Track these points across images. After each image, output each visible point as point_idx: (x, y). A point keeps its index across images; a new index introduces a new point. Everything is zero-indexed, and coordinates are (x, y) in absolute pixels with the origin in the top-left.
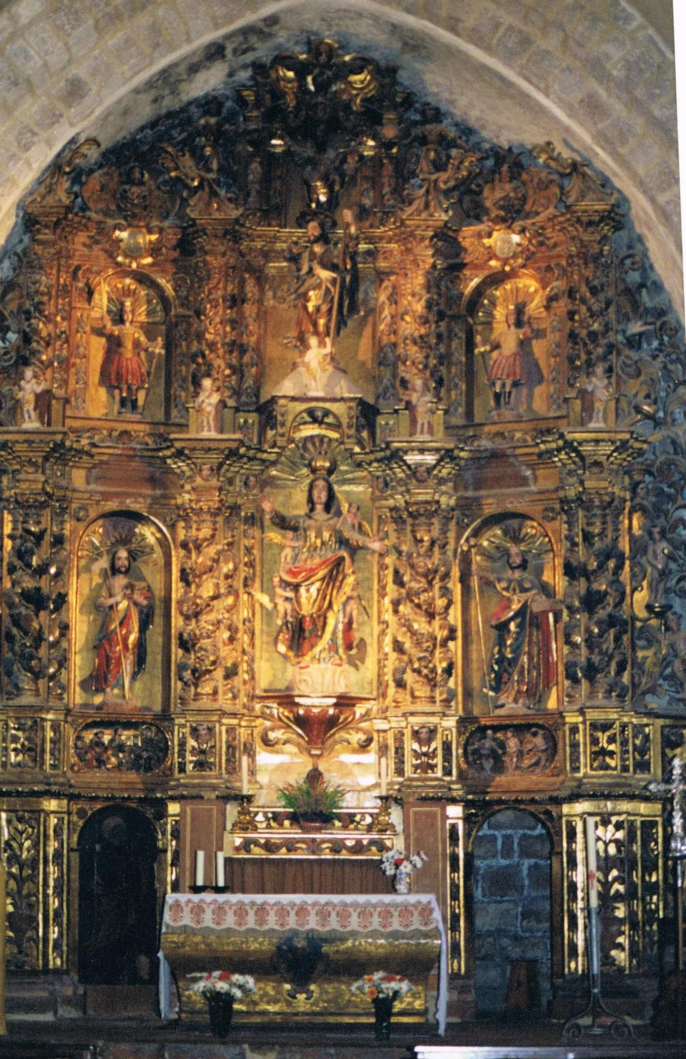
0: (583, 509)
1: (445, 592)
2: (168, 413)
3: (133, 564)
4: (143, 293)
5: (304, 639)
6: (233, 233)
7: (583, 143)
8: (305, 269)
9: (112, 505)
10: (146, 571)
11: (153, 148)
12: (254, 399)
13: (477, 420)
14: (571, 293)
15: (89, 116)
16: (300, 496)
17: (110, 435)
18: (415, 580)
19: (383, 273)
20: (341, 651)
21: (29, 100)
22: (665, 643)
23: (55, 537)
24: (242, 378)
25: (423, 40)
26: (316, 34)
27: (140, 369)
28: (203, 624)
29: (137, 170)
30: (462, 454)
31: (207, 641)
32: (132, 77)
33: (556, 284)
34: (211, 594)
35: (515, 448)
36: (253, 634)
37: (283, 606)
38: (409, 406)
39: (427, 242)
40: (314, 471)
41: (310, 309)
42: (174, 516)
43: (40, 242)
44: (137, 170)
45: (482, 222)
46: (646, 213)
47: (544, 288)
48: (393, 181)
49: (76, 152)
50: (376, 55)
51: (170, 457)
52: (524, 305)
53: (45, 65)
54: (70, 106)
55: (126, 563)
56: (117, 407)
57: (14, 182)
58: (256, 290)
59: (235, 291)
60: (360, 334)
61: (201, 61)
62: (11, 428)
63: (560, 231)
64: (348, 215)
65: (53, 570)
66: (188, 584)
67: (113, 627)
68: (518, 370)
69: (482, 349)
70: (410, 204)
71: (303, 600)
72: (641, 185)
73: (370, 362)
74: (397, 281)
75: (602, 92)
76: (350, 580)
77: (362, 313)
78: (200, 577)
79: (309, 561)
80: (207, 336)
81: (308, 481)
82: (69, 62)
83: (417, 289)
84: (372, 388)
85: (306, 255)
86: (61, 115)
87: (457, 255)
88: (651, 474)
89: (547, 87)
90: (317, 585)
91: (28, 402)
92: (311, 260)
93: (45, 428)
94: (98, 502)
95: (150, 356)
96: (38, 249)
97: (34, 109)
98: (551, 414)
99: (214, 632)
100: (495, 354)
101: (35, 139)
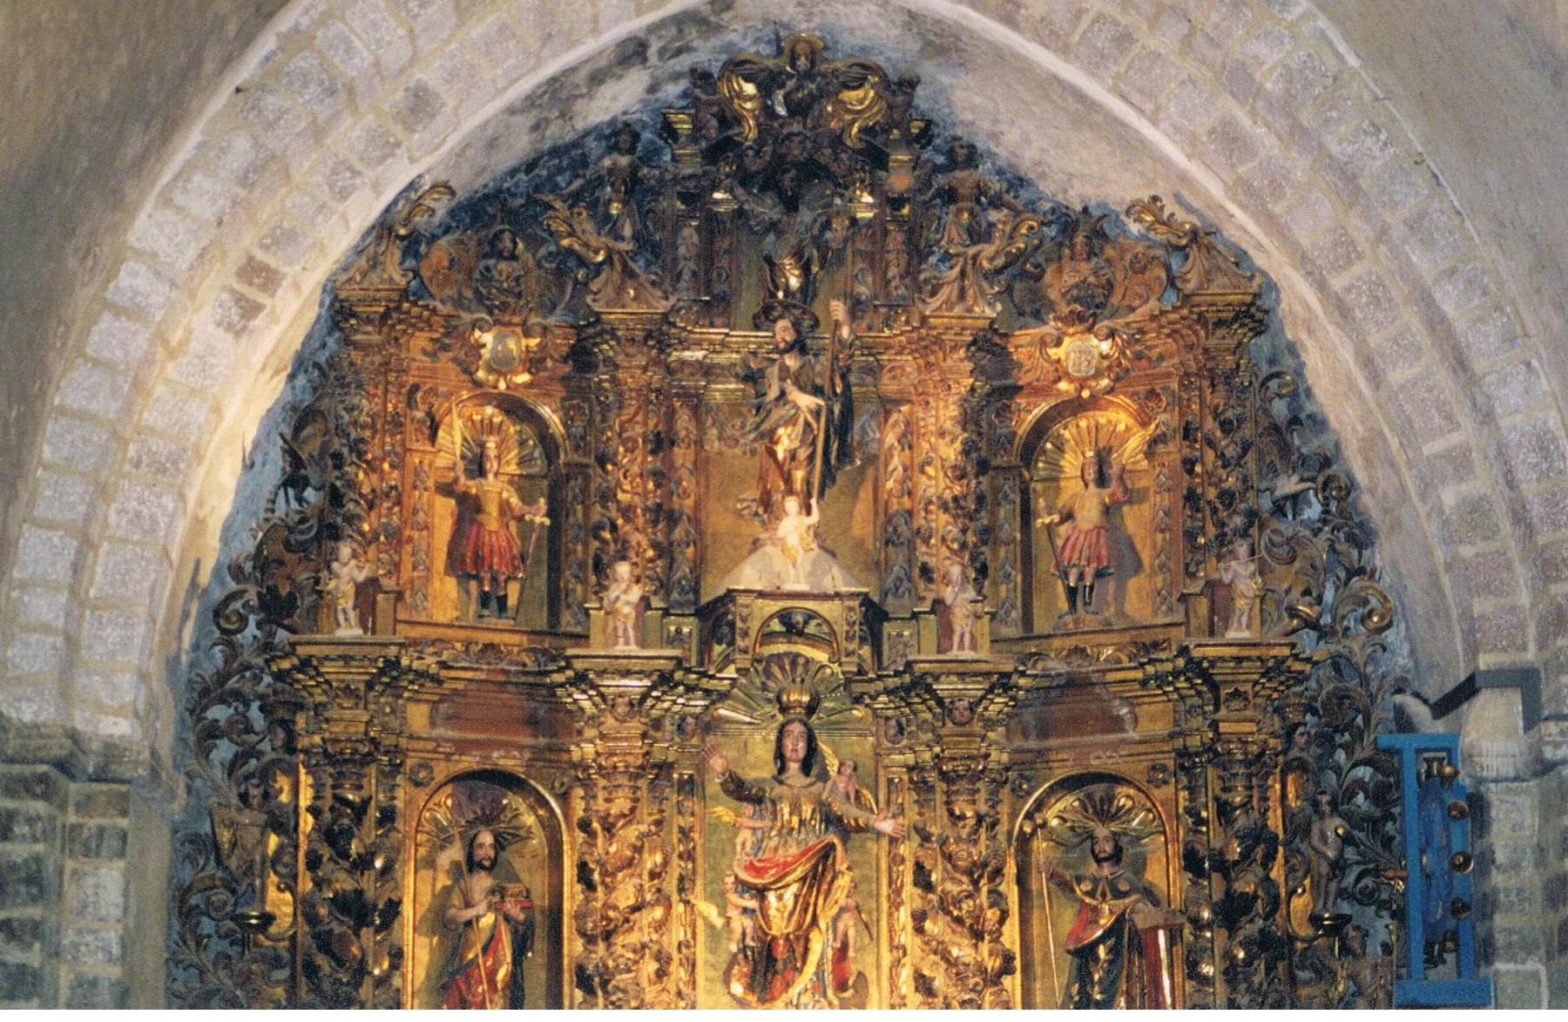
0: (1216, 766)
1: (997, 898)
2: (554, 615)
3: (504, 854)
4: (512, 430)
5: (775, 973)
6: (659, 336)
7: (1207, 196)
8: (773, 393)
9: (470, 762)
10: (519, 865)
11: (531, 201)
12: (691, 596)
13: (1037, 630)
14: (1188, 432)
15: (436, 149)
16: (761, 748)
17: (467, 651)
18: (953, 879)
19: (890, 401)
20: (830, 992)
21: (348, 120)
22: (1342, 973)
23: (383, 811)
24: (671, 564)
25: (958, 38)
26: (786, 27)
27: (511, 548)
28: (619, 950)
29: (507, 236)
30: (1022, 682)
31: (625, 976)
32: (506, 89)
33: (1163, 417)
34: (631, 902)
35: (1104, 672)
36: (694, 965)
37: (740, 923)
38: (939, 606)
39: (962, 353)
40: (784, 709)
41: (780, 456)
42: (566, 780)
43: (357, 346)
44: (507, 236)
45: (1045, 323)
46: (1308, 308)
47: (1144, 425)
48: (904, 258)
49: (417, 203)
50: (880, 60)
51: (562, 685)
52: (1110, 450)
53: (376, 64)
54: (413, 131)
55: (492, 853)
56: (473, 607)
57: (322, 248)
58: (692, 428)
59: (661, 427)
60: (855, 496)
61: (610, 67)
62: (319, 637)
63: (1168, 336)
64: (839, 309)
65: (378, 864)
66: (590, 886)
67: (471, 956)
68: (1104, 553)
69: (1047, 520)
70: (933, 294)
71: (772, 912)
72: (1303, 261)
73: (871, 541)
74: (911, 413)
75: (1245, 120)
76: (844, 881)
77: (859, 463)
78: (613, 875)
79: (781, 852)
80: (620, 496)
81: (776, 725)
82: (413, 60)
83: (948, 425)
84: (873, 580)
85: (773, 372)
86: (398, 144)
87: (1005, 374)
88: (1314, 712)
89: (1158, 109)
90: (794, 888)
91: (344, 595)
92: (782, 379)
93: (369, 638)
94: (448, 756)
95: (526, 528)
96: (356, 356)
97: (355, 135)
98: (1161, 620)
99: (636, 962)
100: (1063, 530)
101: (358, 181)
